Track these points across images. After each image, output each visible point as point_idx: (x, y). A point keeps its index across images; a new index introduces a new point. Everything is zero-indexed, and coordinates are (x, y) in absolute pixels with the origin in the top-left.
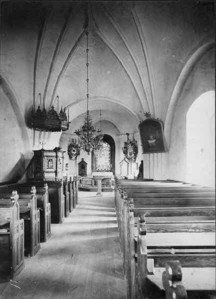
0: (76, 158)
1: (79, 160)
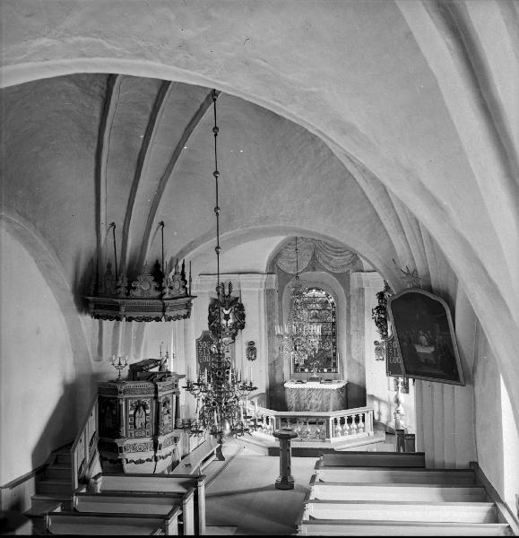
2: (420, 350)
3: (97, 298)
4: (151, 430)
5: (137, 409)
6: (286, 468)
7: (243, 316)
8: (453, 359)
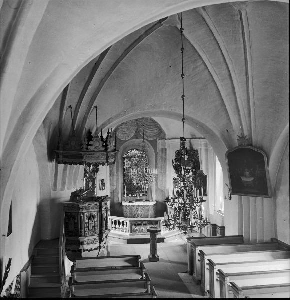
2: (244, 179)
3: (65, 152)
4: (97, 230)
5: (90, 218)
8: (266, 183)
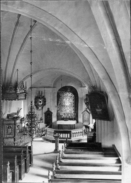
0: (42, 108)
1: (45, 109)
2: (97, 110)
6: (57, 147)
7: (45, 102)
